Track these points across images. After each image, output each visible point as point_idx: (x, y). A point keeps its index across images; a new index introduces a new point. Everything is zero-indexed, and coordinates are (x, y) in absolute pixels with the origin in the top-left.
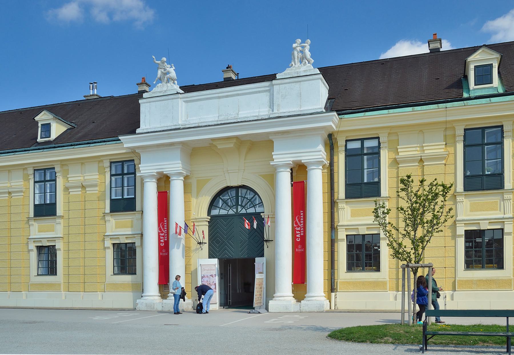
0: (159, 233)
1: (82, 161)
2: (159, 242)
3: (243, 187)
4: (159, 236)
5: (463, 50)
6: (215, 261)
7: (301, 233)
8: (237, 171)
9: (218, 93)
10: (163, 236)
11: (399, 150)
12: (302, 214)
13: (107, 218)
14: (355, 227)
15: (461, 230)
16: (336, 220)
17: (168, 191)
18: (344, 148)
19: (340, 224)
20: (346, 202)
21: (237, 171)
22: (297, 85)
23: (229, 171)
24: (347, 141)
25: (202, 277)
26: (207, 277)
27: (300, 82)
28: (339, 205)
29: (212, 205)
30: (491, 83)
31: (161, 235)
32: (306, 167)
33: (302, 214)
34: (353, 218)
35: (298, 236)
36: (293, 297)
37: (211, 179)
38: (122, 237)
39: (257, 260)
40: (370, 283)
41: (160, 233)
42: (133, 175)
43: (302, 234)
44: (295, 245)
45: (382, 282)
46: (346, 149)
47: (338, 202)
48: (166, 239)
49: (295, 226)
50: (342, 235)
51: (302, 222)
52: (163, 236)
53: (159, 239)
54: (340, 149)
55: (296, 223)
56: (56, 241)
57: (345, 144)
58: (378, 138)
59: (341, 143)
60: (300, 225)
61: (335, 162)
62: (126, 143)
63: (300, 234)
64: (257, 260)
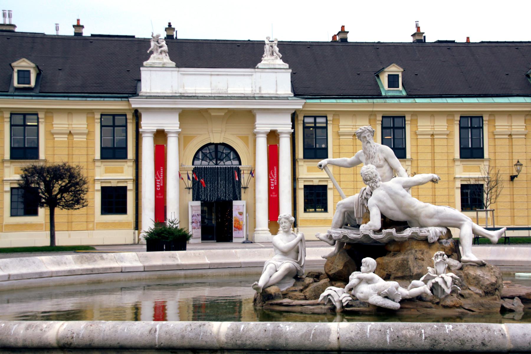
0: (155, 180)
1: (70, 112)
2: (156, 187)
3: (223, 144)
4: (156, 182)
5: (175, 41)
6: (198, 203)
7: (160, 184)
8: (220, 132)
9: (211, 72)
10: (160, 182)
11: (340, 127)
12: (275, 169)
13: (98, 164)
14: (311, 180)
15: (458, 184)
16: (297, 174)
17: (165, 145)
18: (302, 122)
19: (300, 177)
20: (304, 161)
21: (220, 132)
22: (275, 74)
23: (213, 132)
24: (304, 117)
25: (193, 216)
26: (196, 216)
27: (276, 72)
28: (299, 163)
29: (196, 158)
30: (398, 87)
31: (272, 180)
32: (279, 135)
33: (275, 169)
34: (309, 173)
35: (158, 186)
36: (270, 231)
37: (196, 136)
38: (114, 181)
39: (235, 203)
40: (321, 220)
41: (156, 179)
42: (125, 128)
43: (162, 185)
44: (270, 192)
45: (329, 220)
46: (304, 123)
47: (298, 161)
48: (275, 184)
49: (270, 177)
50: (301, 185)
51: (275, 175)
52: (160, 182)
53: (156, 185)
54: (299, 122)
55: (271, 176)
56: (128, 182)
57: (303, 119)
58: (326, 117)
59: (301, 118)
60: (160, 178)
61: (28, 119)
62: (134, 104)
63: (274, 183)
64: (235, 203)
